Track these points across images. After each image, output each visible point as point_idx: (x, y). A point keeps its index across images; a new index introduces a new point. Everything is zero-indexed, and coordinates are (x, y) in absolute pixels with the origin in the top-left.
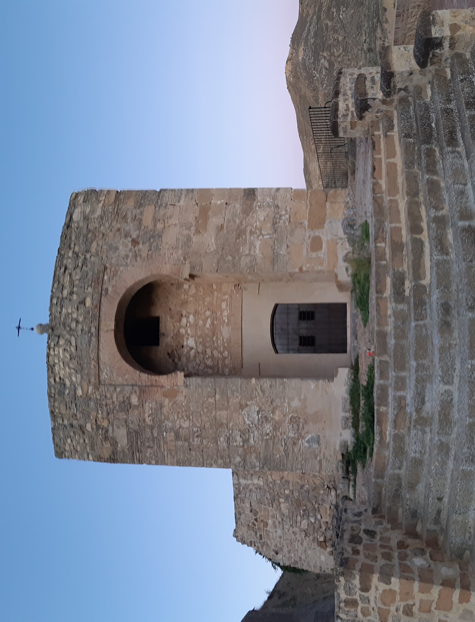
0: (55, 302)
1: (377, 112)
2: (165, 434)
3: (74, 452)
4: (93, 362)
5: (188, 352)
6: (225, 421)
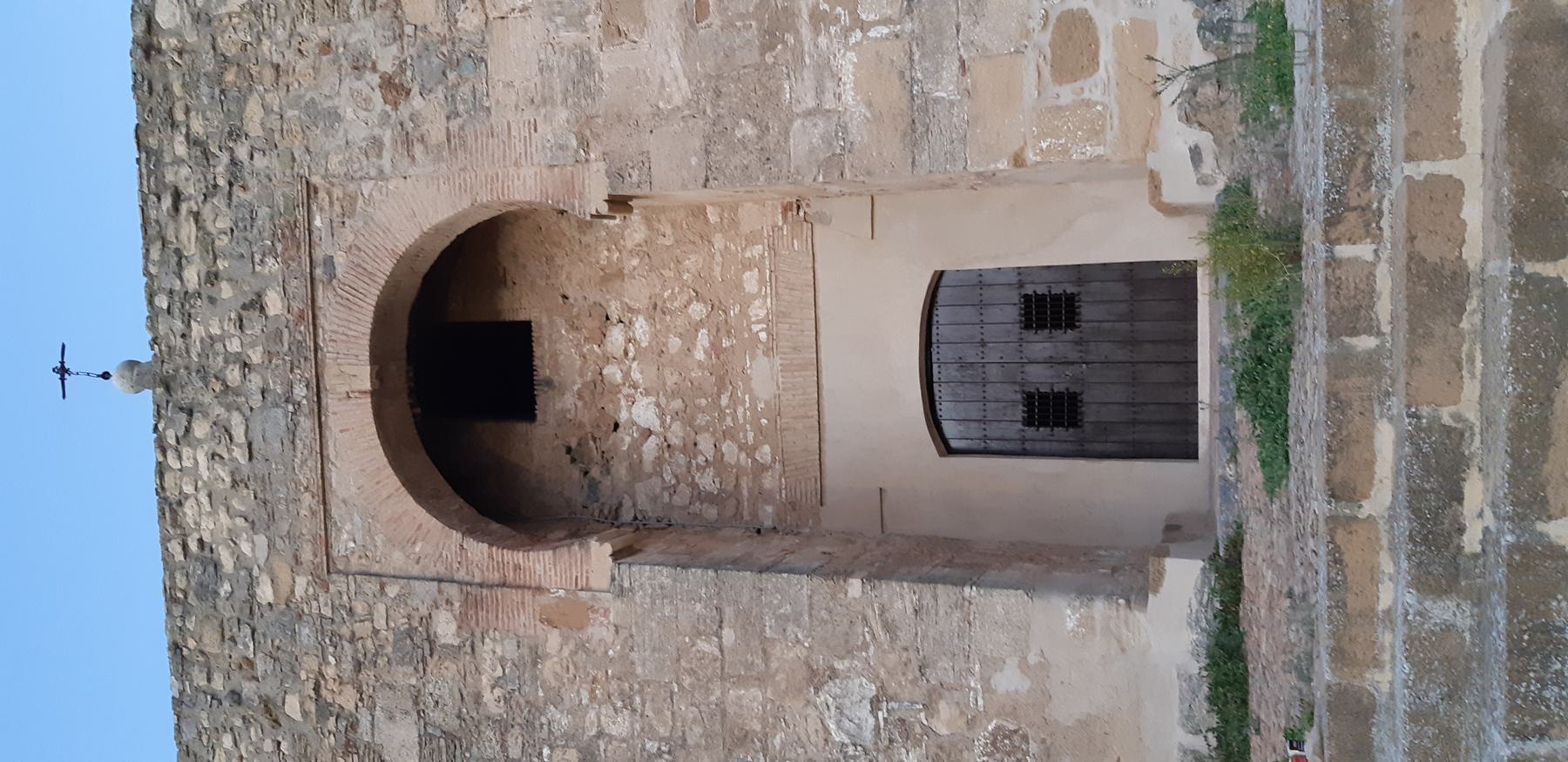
0: (165, 306)
2: (546, 751)
5: (636, 446)
6: (758, 728)
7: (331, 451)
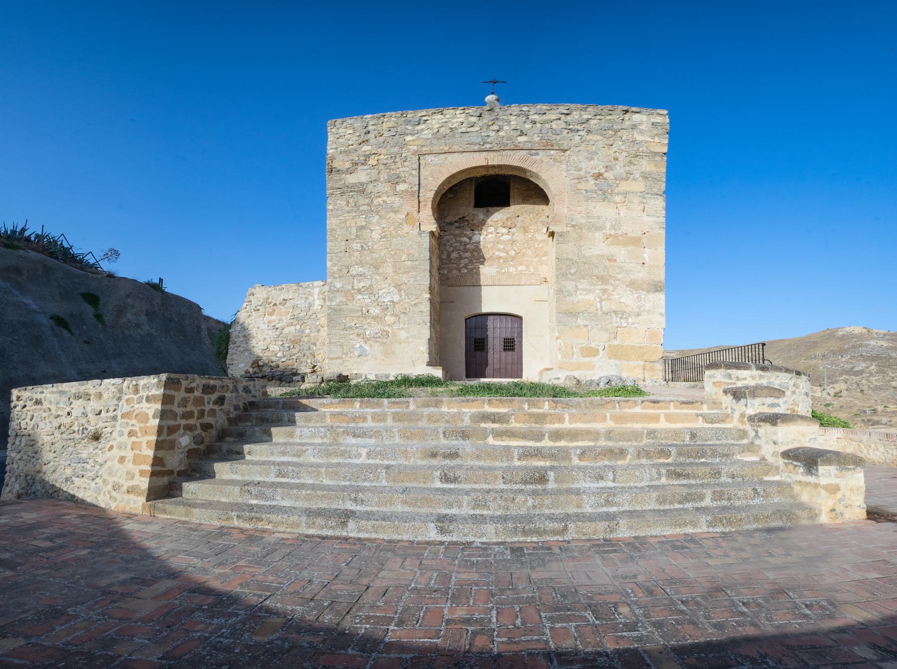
1: (732, 409)
3: (338, 136)
4: (447, 148)
5: (466, 235)
6: (380, 271)
7: (465, 154)
